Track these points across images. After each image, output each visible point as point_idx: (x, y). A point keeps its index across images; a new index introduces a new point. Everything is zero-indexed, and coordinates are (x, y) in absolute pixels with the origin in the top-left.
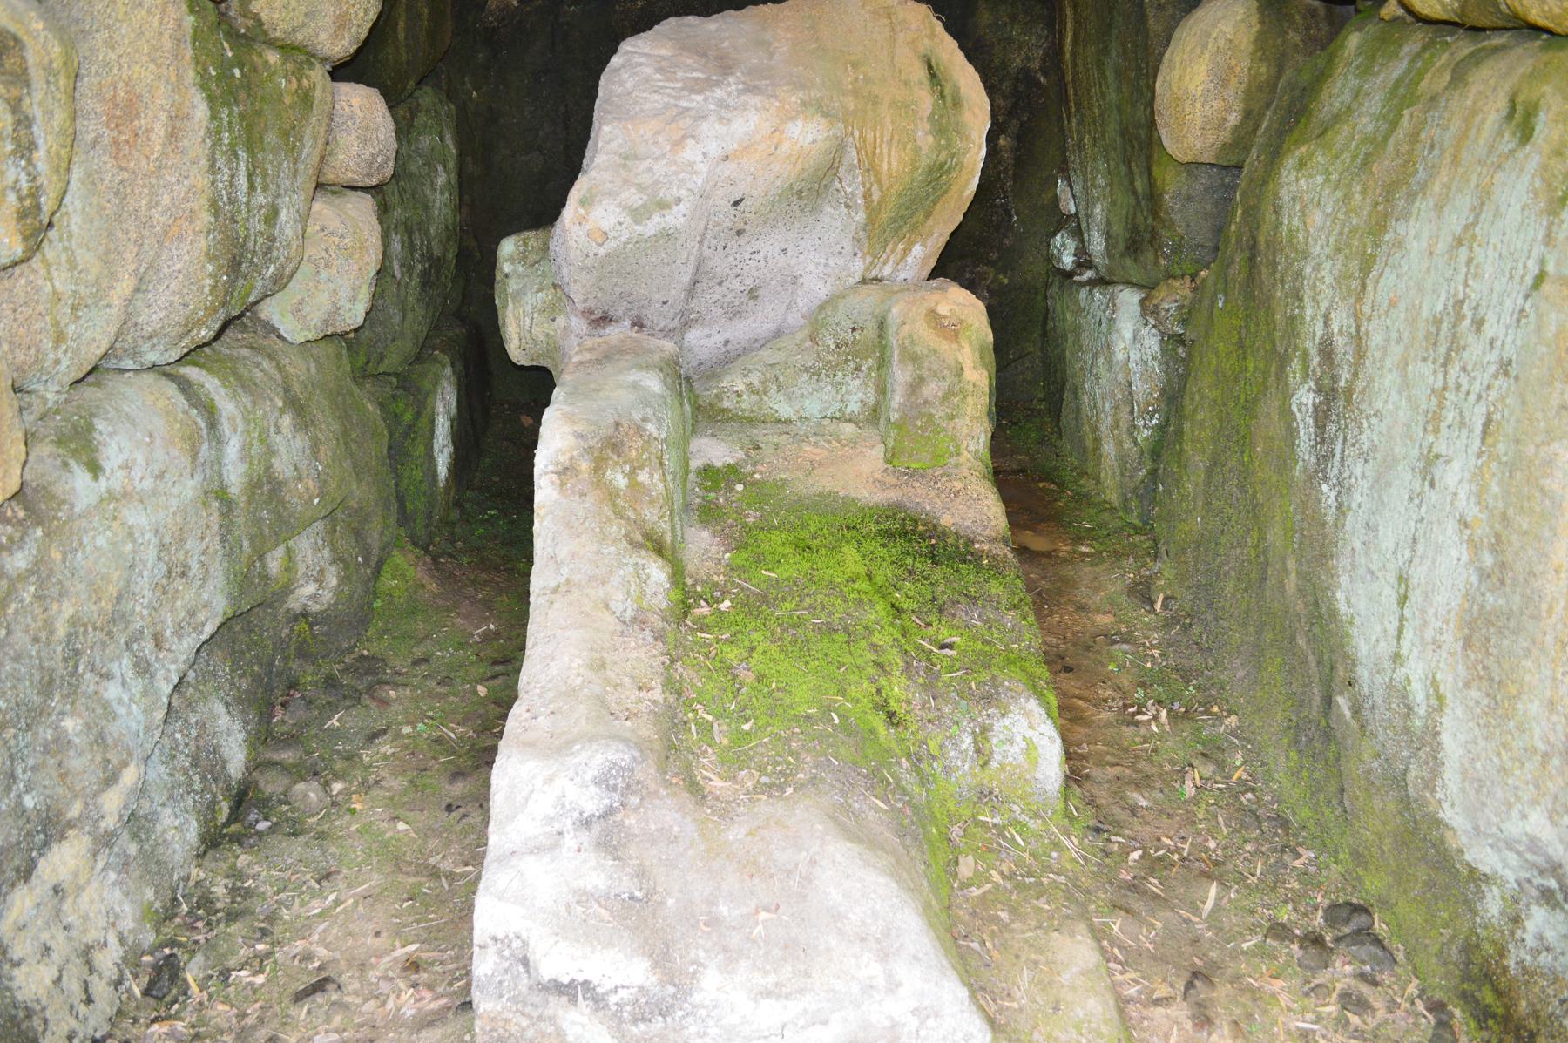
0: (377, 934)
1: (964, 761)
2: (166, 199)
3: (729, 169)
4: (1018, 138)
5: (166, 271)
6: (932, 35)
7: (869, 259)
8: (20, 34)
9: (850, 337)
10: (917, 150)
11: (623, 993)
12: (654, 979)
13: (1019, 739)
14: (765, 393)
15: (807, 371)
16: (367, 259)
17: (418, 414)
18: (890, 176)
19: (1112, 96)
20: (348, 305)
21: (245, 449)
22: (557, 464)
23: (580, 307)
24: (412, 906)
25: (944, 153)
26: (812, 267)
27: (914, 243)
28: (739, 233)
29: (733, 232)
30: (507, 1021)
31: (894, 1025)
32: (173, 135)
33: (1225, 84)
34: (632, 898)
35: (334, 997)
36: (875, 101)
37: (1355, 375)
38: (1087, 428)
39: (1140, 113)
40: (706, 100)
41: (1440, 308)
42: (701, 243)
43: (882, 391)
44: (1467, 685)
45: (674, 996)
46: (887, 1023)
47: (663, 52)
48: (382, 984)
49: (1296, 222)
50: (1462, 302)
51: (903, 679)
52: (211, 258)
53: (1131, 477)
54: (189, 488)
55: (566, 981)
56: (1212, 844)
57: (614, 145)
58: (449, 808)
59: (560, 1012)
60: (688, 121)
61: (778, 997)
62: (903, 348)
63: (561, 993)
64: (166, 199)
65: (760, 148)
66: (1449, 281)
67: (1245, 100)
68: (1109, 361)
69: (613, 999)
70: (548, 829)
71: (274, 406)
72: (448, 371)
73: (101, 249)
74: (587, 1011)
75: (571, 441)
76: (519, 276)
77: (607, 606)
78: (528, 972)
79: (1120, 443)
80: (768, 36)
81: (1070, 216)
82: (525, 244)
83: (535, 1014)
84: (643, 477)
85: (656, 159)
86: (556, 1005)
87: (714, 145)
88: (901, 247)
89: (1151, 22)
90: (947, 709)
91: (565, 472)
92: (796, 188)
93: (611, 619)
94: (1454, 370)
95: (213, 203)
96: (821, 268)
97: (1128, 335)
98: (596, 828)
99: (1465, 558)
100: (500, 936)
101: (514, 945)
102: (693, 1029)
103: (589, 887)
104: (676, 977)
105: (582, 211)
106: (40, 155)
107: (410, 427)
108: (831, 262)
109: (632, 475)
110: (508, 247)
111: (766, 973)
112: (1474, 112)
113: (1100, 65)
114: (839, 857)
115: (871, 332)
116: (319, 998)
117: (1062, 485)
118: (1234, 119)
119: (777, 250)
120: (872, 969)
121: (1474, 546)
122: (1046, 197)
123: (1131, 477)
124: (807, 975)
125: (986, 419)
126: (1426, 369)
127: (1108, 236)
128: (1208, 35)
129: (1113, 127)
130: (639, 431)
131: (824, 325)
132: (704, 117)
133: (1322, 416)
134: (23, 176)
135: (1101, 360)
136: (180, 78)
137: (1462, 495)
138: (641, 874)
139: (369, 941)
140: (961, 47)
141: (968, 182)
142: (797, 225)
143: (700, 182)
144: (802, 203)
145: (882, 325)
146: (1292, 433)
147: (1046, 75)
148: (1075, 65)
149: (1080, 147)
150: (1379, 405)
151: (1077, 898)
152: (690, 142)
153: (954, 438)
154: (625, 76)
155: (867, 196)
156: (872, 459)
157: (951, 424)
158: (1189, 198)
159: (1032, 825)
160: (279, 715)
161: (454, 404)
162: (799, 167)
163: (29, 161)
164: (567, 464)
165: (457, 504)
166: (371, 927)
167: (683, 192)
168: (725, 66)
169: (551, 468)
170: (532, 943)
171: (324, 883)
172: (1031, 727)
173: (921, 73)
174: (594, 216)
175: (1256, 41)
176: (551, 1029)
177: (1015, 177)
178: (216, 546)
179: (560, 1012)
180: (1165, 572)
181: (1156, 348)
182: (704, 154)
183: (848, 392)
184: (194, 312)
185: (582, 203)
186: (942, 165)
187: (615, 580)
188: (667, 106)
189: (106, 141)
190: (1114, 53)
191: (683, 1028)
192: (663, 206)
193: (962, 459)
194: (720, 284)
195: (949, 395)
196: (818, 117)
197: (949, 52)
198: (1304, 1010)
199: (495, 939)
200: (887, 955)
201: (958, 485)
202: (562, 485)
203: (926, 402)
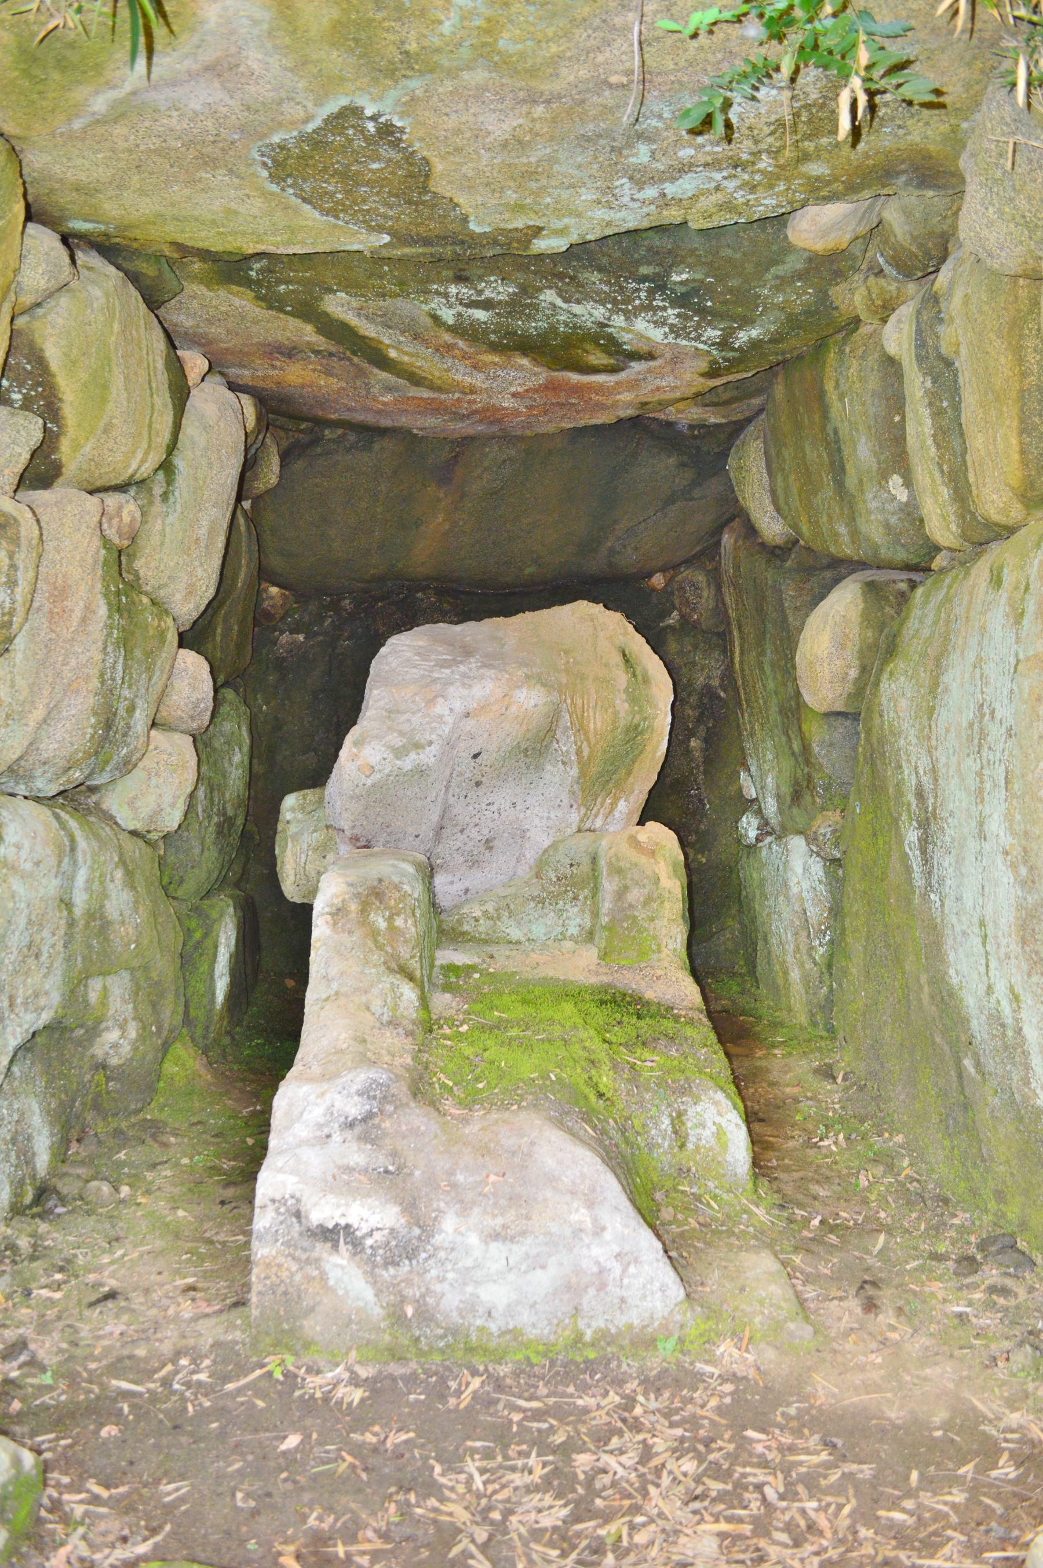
0: (160, 1273)
1: (664, 1139)
2: (73, 662)
3: (470, 724)
4: (706, 740)
5: (64, 714)
6: (625, 633)
7: (583, 811)
8: (19, 517)
9: (568, 872)
10: (616, 714)
11: (378, 1236)
12: (403, 1221)
13: (709, 1124)
14: (499, 919)
15: (533, 899)
16: (186, 776)
17: (206, 935)
18: (596, 734)
19: (771, 685)
20: (168, 809)
21: (89, 881)
22: (332, 905)
23: (348, 833)
24: (190, 1259)
25: (637, 717)
26: (537, 821)
27: (619, 799)
28: (478, 784)
29: (473, 783)
30: (280, 1266)
31: (602, 1271)
32: (84, 620)
33: (843, 646)
34: (386, 1172)
35: (123, 1304)
36: (583, 678)
37: (936, 797)
38: (777, 967)
39: (791, 691)
40: (453, 672)
41: (971, 715)
42: (447, 788)
43: (595, 915)
44: (1029, 975)
45: (419, 1238)
46: (595, 1269)
47: (421, 643)
48: (164, 1300)
49: (892, 714)
50: (982, 705)
51: (611, 1073)
52: (95, 714)
53: (815, 994)
54: (51, 886)
55: (331, 1226)
56: (882, 1215)
57: (382, 703)
58: (223, 1203)
59: (325, 1255)
60: (439, 686)
61: (505, 1240)
62: (610, 865)
63: (326, 1239)
64: (73, 662)
65: (495, 708)
66: (972, 695)
67: (859, 658)
68: (787, 898)
69: (369, 1242)
70: (318, 1133)
71: (112, 858)
72: (231, 910)
73: (31, 680)
74: (346, 1255)
75: (343, 887)
76: (298, 821)
77: (368, 1009)
78: (300, 1222)
79: (802, 965)
80: (500, 634)
81: (752, 801)
82: (304, 798)
83: (304, 1256)
84: (399, 922)
85: (413, 713)
86: (321, 1249)
87: (458, 704)
88: (608, 801)
89: (791, 619)
90: (648, 1096)
91: (338, 912)
92: (523, 747)
93: (371, 1018)
94: (985, 752)
95: (102, 675)
96: (544, 821)
97: (799, 870)
98: (358, 1129)
99: (1012, 880)
100: (278, 1197)
101: (289, 1203)
102: (434, 1273)
103: (352, 1163)
104: (422, 1223)
105: (355, 750)
106: (18, 590)
107: (198, 942)
108: (552, 815)
109: (390, 920)
110: (290, 801)
111: (494, 1216)
112: (973, 587)
113: (760, 664)
114: (553, 1138)
115: (585, 867)
116: (110, 1304)
117: (759, 1018)
118: (853, 673)
119: (508, 804)
120: (581, 1215)
121: (1014, 866)
122: (733, 789)
123: (815, 994)
124: (528, 1218)
125: (681, 921)
126: (970, 761)
127: (778, 797)
128: (828, 615)
129: (774, 709)
130: (397, 888)
131: (547, 863)
132: (452, 684)
133: (924, 843)
134: (8, 599)
135: (781, 898)
136: (93, 586)
137: (1002, 834)
138: (394, 1154)
139: (152, 1277)
140: (648, 642)
141: (659, 742)
142: (524, 781)
143: (447, 731)
144: (528, 760)
145: (594, 860)
146: (909, 870)
147: (725, 691)
148: (742, 670)
149: (752, 734)
150: (951, 806)
151: (766, 1241)
152: (440, 700)
153: (655, 937)
154: (390, 659)
155: (579, 752)
156: (590, 955)
157: (652, 926)
158: (831, 745)
159: (725, 1196)
160: (74, 1147)
161: (233, 942)
162: (524, 727)
163: (12, 592)
164: (340, 905)
165: (228, 1033)
166: (155, 1269)
167: (434, 737)
168: (467, 652)
169: (327, 910)
170: (304, 1199)
171: (114, 1243)
172: (720, 1114)
173: (618, 659)
174: (363, 755)
175: (862, 616)
176: (316, 1273)
177: (705, 773)
178: (60, 947)
179: (325, 1255)
180: (843, 1060)
181: (821, 873)
182: (451, 710)
183: (568, 918)
184: (77, 751)
185: (355, 744)
186: (637, 726)
187: (375, 991)
188: (423, 677)
189: (46, 609)
190: (768, 652)
191: (426, 1271)
192: (418, 746)
193: (663, 956)
194: (462, 831)
195: (648, 900)
196: (538, 686)
197: (639, 646)
198: (958, 1299)
199: (273, 1201)
200: (593, 1204)
201: (659, 972)
202: (335, 924)
203: (631, 906)
